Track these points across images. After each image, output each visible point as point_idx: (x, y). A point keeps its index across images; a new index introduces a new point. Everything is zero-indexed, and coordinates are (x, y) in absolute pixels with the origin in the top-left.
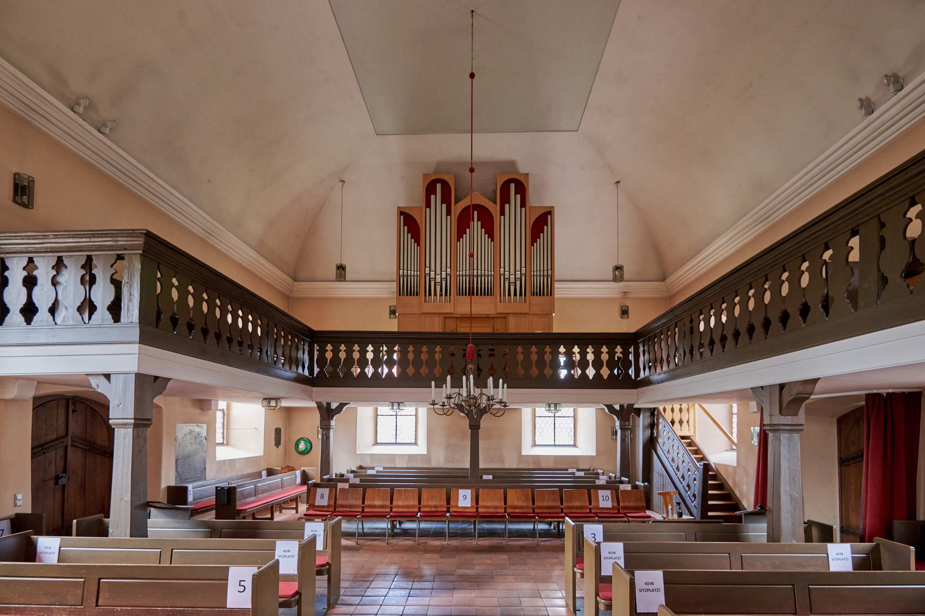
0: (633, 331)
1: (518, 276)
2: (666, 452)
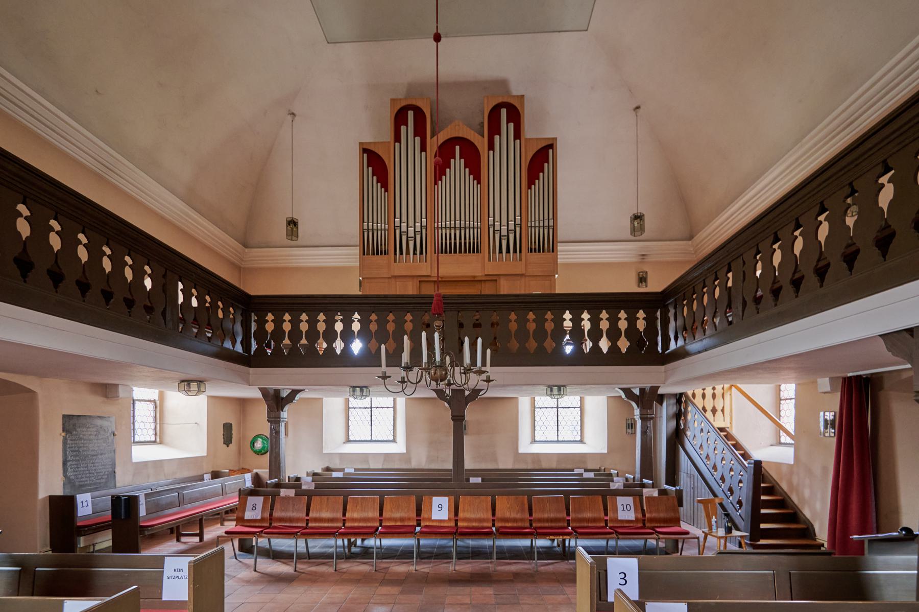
0: (660, 290)
1: (512, 227)
2: (697, 448)
